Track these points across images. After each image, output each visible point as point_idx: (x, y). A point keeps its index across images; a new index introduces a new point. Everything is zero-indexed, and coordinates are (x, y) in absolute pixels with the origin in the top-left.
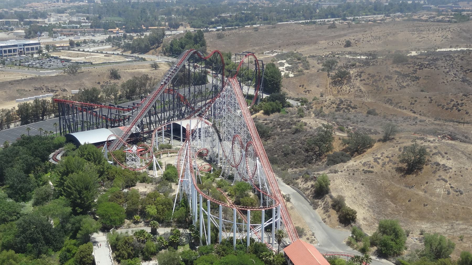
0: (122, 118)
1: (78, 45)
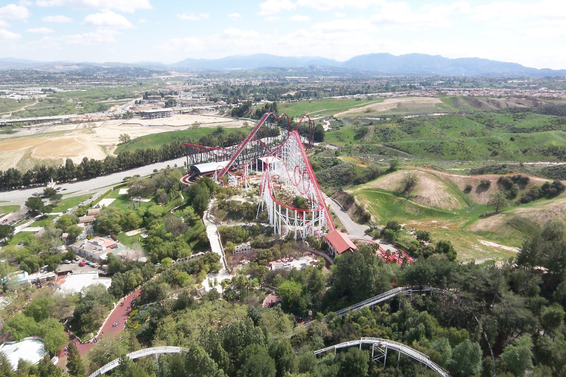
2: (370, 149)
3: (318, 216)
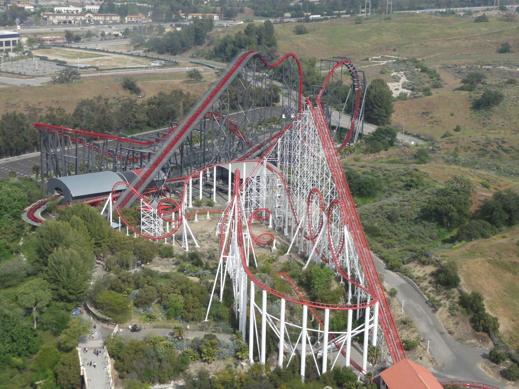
0: (139, 156)
1: (77, 39)
2: (506, 146)
3: (362, 320)
